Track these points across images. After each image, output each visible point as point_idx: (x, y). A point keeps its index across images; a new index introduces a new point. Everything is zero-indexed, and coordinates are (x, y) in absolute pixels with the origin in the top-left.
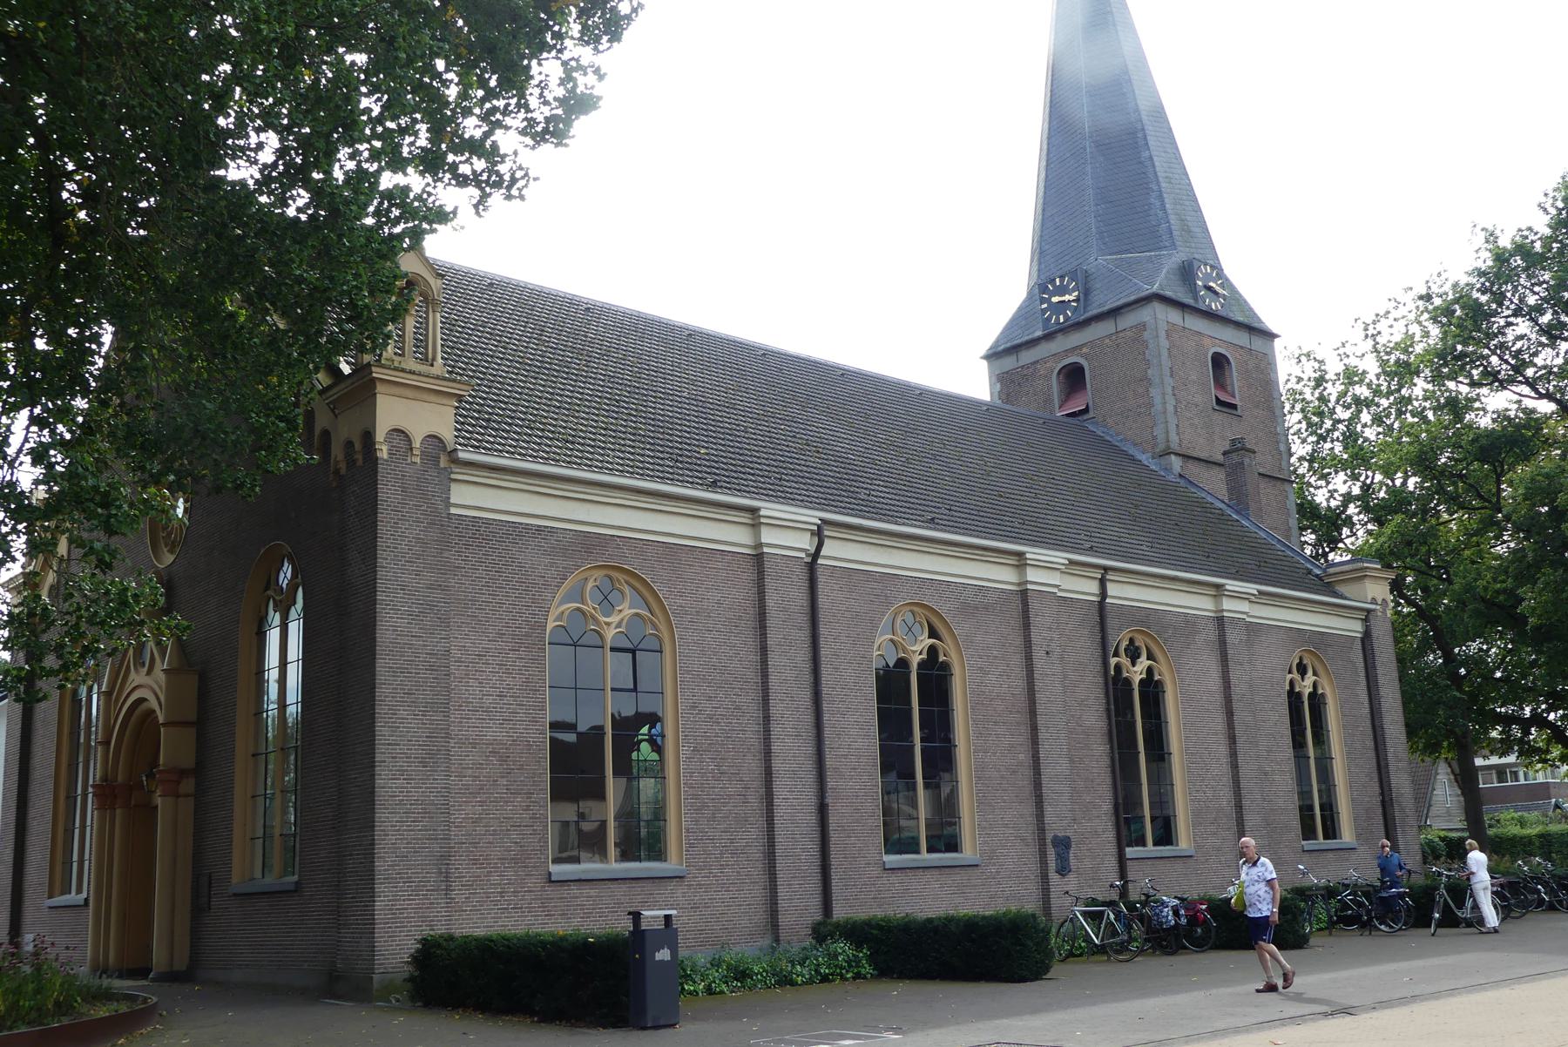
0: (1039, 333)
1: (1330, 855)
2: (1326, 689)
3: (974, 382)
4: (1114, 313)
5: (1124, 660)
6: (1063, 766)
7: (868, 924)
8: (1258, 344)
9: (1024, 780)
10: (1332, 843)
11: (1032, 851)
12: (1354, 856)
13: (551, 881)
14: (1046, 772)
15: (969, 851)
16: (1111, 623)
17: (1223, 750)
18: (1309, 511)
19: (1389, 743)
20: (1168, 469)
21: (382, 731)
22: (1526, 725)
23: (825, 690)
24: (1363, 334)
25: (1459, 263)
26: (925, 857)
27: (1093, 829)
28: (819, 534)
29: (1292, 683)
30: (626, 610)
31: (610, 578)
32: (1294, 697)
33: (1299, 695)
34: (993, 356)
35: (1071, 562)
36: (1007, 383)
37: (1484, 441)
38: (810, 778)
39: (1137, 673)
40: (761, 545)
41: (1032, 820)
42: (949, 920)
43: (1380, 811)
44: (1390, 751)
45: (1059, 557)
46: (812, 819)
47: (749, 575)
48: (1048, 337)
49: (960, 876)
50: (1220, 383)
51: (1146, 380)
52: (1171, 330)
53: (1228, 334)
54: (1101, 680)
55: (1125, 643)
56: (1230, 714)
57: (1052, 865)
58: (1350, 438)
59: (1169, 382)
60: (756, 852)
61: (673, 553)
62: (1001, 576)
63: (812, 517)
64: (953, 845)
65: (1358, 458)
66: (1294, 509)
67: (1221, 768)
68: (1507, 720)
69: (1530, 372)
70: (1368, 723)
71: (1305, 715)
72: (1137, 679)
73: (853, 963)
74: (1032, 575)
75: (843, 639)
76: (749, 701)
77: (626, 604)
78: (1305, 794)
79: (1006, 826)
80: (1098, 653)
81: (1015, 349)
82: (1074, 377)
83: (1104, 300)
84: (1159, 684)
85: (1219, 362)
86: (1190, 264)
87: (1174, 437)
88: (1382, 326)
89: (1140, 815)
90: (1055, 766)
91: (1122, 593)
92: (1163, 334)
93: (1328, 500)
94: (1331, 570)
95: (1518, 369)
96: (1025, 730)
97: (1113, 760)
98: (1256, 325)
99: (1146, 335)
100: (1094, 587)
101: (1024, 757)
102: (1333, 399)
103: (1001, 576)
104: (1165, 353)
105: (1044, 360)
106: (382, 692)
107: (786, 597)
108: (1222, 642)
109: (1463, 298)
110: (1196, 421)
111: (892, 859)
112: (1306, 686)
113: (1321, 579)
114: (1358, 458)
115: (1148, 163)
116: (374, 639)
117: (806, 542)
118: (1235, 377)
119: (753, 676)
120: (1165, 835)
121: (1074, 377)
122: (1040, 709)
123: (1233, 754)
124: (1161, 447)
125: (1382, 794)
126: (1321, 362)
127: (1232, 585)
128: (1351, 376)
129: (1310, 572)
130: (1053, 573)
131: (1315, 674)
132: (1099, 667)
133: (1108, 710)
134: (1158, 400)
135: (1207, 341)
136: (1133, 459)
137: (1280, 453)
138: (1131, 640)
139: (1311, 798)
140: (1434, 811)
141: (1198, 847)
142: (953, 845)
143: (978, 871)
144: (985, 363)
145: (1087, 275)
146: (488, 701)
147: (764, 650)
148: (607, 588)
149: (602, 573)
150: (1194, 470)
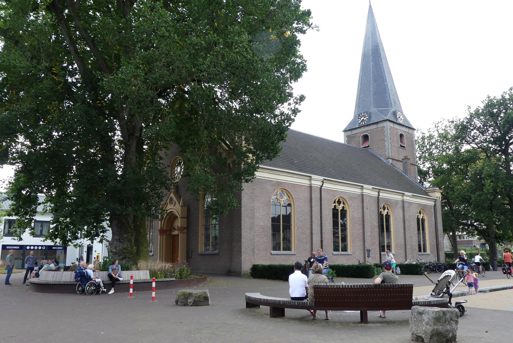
0: (357, 126)
2: (425, 217)
3: (340, 138)
4: (377, 123)
5: (382, 210)
7: (334, 266)
12: (430, 256)
14: (366, 234)
15: (349, 251)
16: (380, 201)
17: (402, 231)
19: (439, 230)
21: (243, 222)
22: (468, 226)
25: (462, 116)
27: (376, 248)
28: (323, 182)
32: (418, 219)
34: (345, 131)
36: (349, 138)
37: (465, 159)
38: (320, 235)
39: (385, 213)
45: (370, 187)
46: (320, 243)
47: (309, 190)
48: (360, 127)
49: (347, 257)
50: (401, 141)
53: (404, 129)
54: (377, 214)
56: (404, 223)
57: (366, 255)
58: (431, 154)
61: (294, 186)
62: (358, 191)
63: (322, 178)
64: (346, 250)
65: (431, 157)
68: (464, 224)
69: (476, 141)
71: (420, 224)
74: (364, 191)
76: (308, 218)
78: (419, 242)
81: (349, 130)
83: (374, 120)
86: (396, 111)
87: (390, 154)
88: (440, 125)
89: (340, 242)
90: (368, 234)
91: (383, 195)
95: (473, 141)
96: (362, 225)
99: (385, 129)
100: (377, 194)
101: (361, 231)
102: (426, 143)
103: (358, 191)
105: (359, 133)
106: (243, 215)
107: (316, 195)
108: (403, 207)
109: (462, 124)
111: (335, 253)
112: (421, 217)
114: (431, 157)
117: (321, 184)
118: (405, 139)
119: (309, 213)
122: (365, 221)
123: (405, 232)
124: (387, 157)
127: (406, 193)
130: (369, 191)
132: (377, 212)
134: (387, 145)
135: (399, 131)
142: (289, 249)
145: (370, 113)
146: (260, 217)
147: (311, 207)
150: (395, 162)
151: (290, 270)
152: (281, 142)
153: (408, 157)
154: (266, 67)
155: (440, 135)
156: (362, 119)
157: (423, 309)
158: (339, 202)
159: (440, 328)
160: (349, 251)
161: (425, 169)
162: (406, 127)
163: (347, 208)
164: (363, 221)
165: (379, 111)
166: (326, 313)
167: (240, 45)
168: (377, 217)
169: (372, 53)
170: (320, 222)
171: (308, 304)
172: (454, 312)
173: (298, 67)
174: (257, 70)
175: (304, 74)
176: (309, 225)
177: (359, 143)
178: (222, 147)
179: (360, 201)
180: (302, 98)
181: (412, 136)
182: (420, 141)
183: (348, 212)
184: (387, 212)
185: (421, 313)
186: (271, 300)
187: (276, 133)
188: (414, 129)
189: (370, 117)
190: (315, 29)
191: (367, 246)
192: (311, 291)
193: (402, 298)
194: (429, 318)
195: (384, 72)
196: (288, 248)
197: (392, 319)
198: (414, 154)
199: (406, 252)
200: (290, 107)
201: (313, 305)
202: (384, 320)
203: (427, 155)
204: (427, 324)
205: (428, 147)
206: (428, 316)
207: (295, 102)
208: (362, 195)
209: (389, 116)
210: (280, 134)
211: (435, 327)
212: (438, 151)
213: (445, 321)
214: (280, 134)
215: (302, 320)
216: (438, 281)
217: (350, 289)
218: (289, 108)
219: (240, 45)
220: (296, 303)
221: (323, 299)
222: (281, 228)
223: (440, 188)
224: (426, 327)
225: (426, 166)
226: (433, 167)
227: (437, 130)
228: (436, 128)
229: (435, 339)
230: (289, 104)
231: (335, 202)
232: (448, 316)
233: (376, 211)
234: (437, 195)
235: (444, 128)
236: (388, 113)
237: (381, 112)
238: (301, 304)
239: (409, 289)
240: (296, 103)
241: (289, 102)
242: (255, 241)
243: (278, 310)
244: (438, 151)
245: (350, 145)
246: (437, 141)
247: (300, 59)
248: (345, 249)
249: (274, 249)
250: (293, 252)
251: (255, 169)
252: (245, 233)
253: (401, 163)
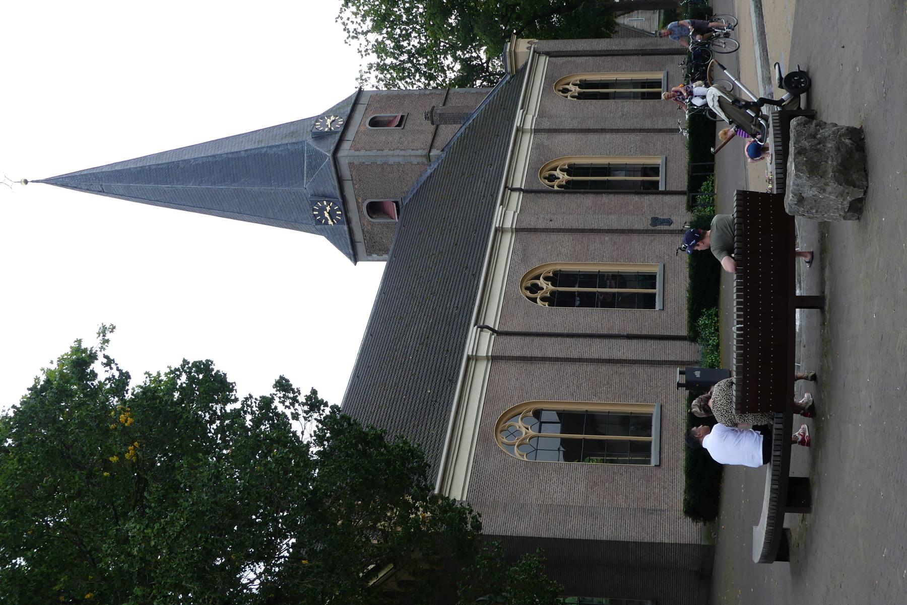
0: (346, 228)
2: (577, 79)
3: (373, 271)
5: (556, 183)
6: (613, 218)
8: (364, 100)
9: (621, 238)
10: (664, 84)
11: (659, 238)
12: (671, 73)
13: (659, 465)
14: (615, 226)
15: (656, 269)
16: (535, 187)
17: (608, 136)
18: (464, 80)
19: (609, 48)
20: (438, 157)
23: (566, 331)
24: (355, 40)
26: (658, 290)
27: (647, 201)
28: (483, 328)
29: (573, 97)
30: (519, 424)
31: (502, 431)
32: (581, 96)
33: (579, 93)
34: (355, 259)
35: (501, 204)
36: (373, 251)
38: (613, 341)
39: (563, 177)
40: (487, 356)
41: (641, 237)
42: (691, 265)
43: (647, 57)
44: (614, 48)
45: (499, 210)
46: (634, 342)
47: (503, 365)
48: (349, 222)
49: (669, 274)
50: (388, 123)
51: (383, 166)
55: (546, 181)
57: (666, 227)
58: (421, 52)
59: (385, 152)
60: (650, 370)
61: (490, 399)
62: (507, 242)
63: (473, 330)
66: (462, 90)
67: (618, 138)
70: (598, 58)
71: (592, 91)
72: (566, 177)
73: (709, 317)
75: (539, 321)
77: (517, 425)
78: (635, 96)
79: (644, 249)
80: (552, 196)
82: (375, 209)
83: (331, 186)
84: (570, 166)
86: (314, 133)
87: (419, 152)
88: (351, 27)
89: (646, 182)
90: (613, 222)
91: (519, 181)
92: (357, 153)
93: (454, 71)
94: (509, 70)
96: (592, 236)
97: (610, 193)
100: (515, 195)
101: (607, 238)
102: (394, 61)
103: (507, 242)
104: (368, 153)
105: (362, 226)
107: (515, 347)
111: (658, 305)
112: (575, 90)
113: (513, 76)
115: (249, 153)
116: (531, 538)
117: (486, 334)
120: (655, 170)
121: (375, 209)
122: (582, 227)
124: (424, 160)
125: (638, 55)
127: (517, 122)
128: (380, 49)
129: (508, 82)
130: (508, 214)
131: (568, 84)
133: (584, 193)
134: (397, 160)
135: (362, 129)
136: (431, 176)
138: (545, 178)
139: (638, 93)
140: (647, 28)
141: (661, 154)
143: (667, 265)
147: (544, 359)
148: (507, 433)
149: (499, 434)
150: (439, 143)
151: (699, 459)
152: (387, 439)
153: (428, 109)
154: (209, 480)
155: (377, 28)
156: (327, 215)
157: (791, 195)
158: (535, 288)
159: (831, 165)
160: (655, 268)
161: (458, 66)
162: (353, 110)
163: (549, 270)
164: (583, 231)
165: (310, 175)
166: (801, 378)
167: (153, 543)
168: (574, 197)
169: (167, 183)
170: (581, 340)
171: (780, 426)
172: (799, 128)
173: (199, 383)
174: (216, 503)
175: (218, 367)
176: (589, 368)
177: (387, 225)
178: (384, 581)
179: (533, 236)
180: (283, 385)
181: (376, 96)
182: (389, 76)
183: (558, 268)
184: (562, 170)
185: (801, 200)
186: (770, 509)
187: (364, 453)
188: (360, 92)
189: (325, 196)
190: (109, 336)
191: (645, 224)
192: (751, 420)
193: (765, 225)
194: (811, 187)
195: (214, 156)
196: (642, 424)
197: (815, 236)
198: (421, 95)
199: (661, 131)
200: (302, 414)
201: (781, 415)
202: (817, 256)
203: (423, 61)
204: (824, 191)
205: (405, 57)
206: (807, 188)
207: (292, 404)
208: (518, 230)
209: (326, 149)
210: (367, 443)
211: (830, 174)
212: (414, 34)
213: (818, 151)
214: (367, 443)
215: (815, 443)
216: (731, 123)
217: (746, 300)
218: (305, 418)
219: (153, 543)
220: (778, 453)
221: (767, 399)
222: (590, 437)
223: (508, 35)
224: (830, 193)
225: (452, 67)
226: (453, 48)
227: (365, 33)
228: (360, 36)
229: (855, 176)
230: (295, 416)
231: (534, 300)
232: (806, 144)
233: (559, 197)
234: (523, 47)
235: (359, 18)
236: (317, 152)
237: (313, 168)
238: (779, 443)
239: (747, 199)
240: (295, 400)
241: (290, 416)
242: (624, 505)
243: (794, 494)
244: (414, 34)
245: (392, 247)
246: (390, 36)
247: (179, 377)
248: (649, 280)
250: (655, 411)
251: (450, 504)
252: (606, 530)
253: (443, 127)
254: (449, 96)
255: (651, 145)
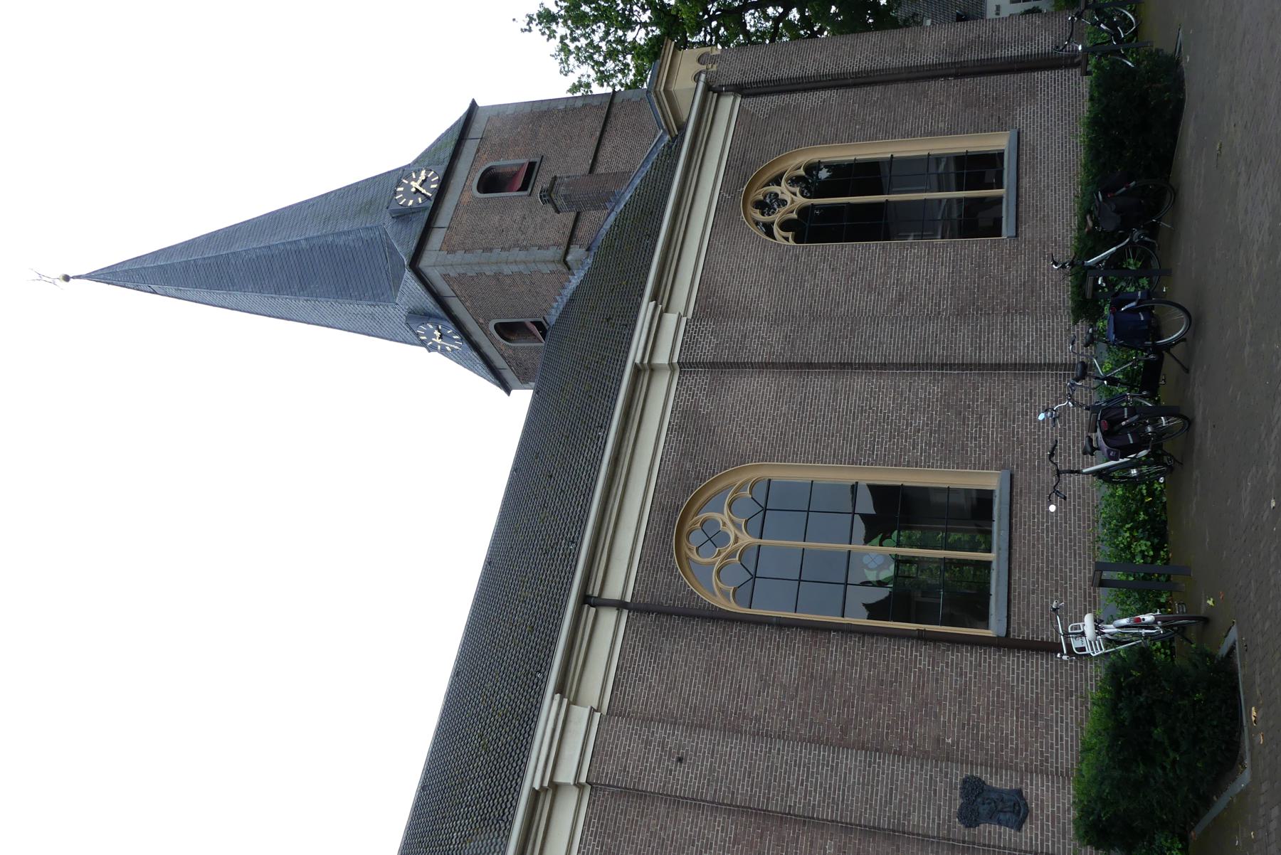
1: (1025, 182)
2: (797, 162)
8: (477, 130)
12: (1028, 137)
17: (859, 382)
34: (508, 391)
35: (561, 689)
36: (524, 380)
51: (497, 276)
52: (449, 248)
70: (851, 93)
85: (491, 182)
89: (972, 200)
98: (456, 136)
104: (468, 256)
105: (499, 351)
110: (539, 220)
111: (1007, 228)
112: (794, 199)
121: (508, 330)
125: (946, 76)
126: (531, 19)
127: (635, 354)
131: (777, 181)
134: (515, 268)
135: (466, 198)
137: (584, 106)
144: (513, 392)
249: (995, 230)
254: (614, 110)
255: (972, 421)
